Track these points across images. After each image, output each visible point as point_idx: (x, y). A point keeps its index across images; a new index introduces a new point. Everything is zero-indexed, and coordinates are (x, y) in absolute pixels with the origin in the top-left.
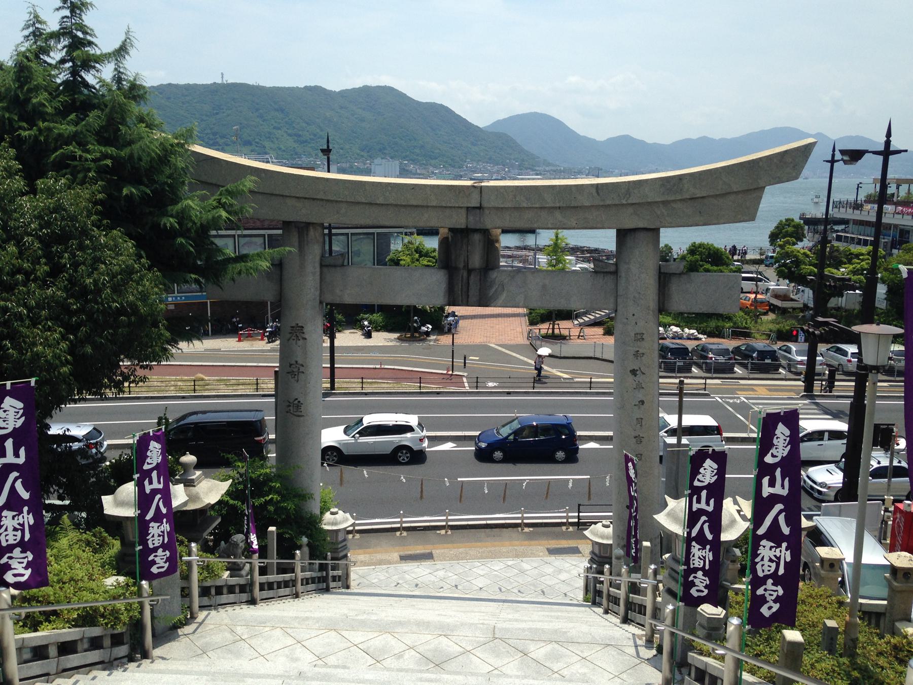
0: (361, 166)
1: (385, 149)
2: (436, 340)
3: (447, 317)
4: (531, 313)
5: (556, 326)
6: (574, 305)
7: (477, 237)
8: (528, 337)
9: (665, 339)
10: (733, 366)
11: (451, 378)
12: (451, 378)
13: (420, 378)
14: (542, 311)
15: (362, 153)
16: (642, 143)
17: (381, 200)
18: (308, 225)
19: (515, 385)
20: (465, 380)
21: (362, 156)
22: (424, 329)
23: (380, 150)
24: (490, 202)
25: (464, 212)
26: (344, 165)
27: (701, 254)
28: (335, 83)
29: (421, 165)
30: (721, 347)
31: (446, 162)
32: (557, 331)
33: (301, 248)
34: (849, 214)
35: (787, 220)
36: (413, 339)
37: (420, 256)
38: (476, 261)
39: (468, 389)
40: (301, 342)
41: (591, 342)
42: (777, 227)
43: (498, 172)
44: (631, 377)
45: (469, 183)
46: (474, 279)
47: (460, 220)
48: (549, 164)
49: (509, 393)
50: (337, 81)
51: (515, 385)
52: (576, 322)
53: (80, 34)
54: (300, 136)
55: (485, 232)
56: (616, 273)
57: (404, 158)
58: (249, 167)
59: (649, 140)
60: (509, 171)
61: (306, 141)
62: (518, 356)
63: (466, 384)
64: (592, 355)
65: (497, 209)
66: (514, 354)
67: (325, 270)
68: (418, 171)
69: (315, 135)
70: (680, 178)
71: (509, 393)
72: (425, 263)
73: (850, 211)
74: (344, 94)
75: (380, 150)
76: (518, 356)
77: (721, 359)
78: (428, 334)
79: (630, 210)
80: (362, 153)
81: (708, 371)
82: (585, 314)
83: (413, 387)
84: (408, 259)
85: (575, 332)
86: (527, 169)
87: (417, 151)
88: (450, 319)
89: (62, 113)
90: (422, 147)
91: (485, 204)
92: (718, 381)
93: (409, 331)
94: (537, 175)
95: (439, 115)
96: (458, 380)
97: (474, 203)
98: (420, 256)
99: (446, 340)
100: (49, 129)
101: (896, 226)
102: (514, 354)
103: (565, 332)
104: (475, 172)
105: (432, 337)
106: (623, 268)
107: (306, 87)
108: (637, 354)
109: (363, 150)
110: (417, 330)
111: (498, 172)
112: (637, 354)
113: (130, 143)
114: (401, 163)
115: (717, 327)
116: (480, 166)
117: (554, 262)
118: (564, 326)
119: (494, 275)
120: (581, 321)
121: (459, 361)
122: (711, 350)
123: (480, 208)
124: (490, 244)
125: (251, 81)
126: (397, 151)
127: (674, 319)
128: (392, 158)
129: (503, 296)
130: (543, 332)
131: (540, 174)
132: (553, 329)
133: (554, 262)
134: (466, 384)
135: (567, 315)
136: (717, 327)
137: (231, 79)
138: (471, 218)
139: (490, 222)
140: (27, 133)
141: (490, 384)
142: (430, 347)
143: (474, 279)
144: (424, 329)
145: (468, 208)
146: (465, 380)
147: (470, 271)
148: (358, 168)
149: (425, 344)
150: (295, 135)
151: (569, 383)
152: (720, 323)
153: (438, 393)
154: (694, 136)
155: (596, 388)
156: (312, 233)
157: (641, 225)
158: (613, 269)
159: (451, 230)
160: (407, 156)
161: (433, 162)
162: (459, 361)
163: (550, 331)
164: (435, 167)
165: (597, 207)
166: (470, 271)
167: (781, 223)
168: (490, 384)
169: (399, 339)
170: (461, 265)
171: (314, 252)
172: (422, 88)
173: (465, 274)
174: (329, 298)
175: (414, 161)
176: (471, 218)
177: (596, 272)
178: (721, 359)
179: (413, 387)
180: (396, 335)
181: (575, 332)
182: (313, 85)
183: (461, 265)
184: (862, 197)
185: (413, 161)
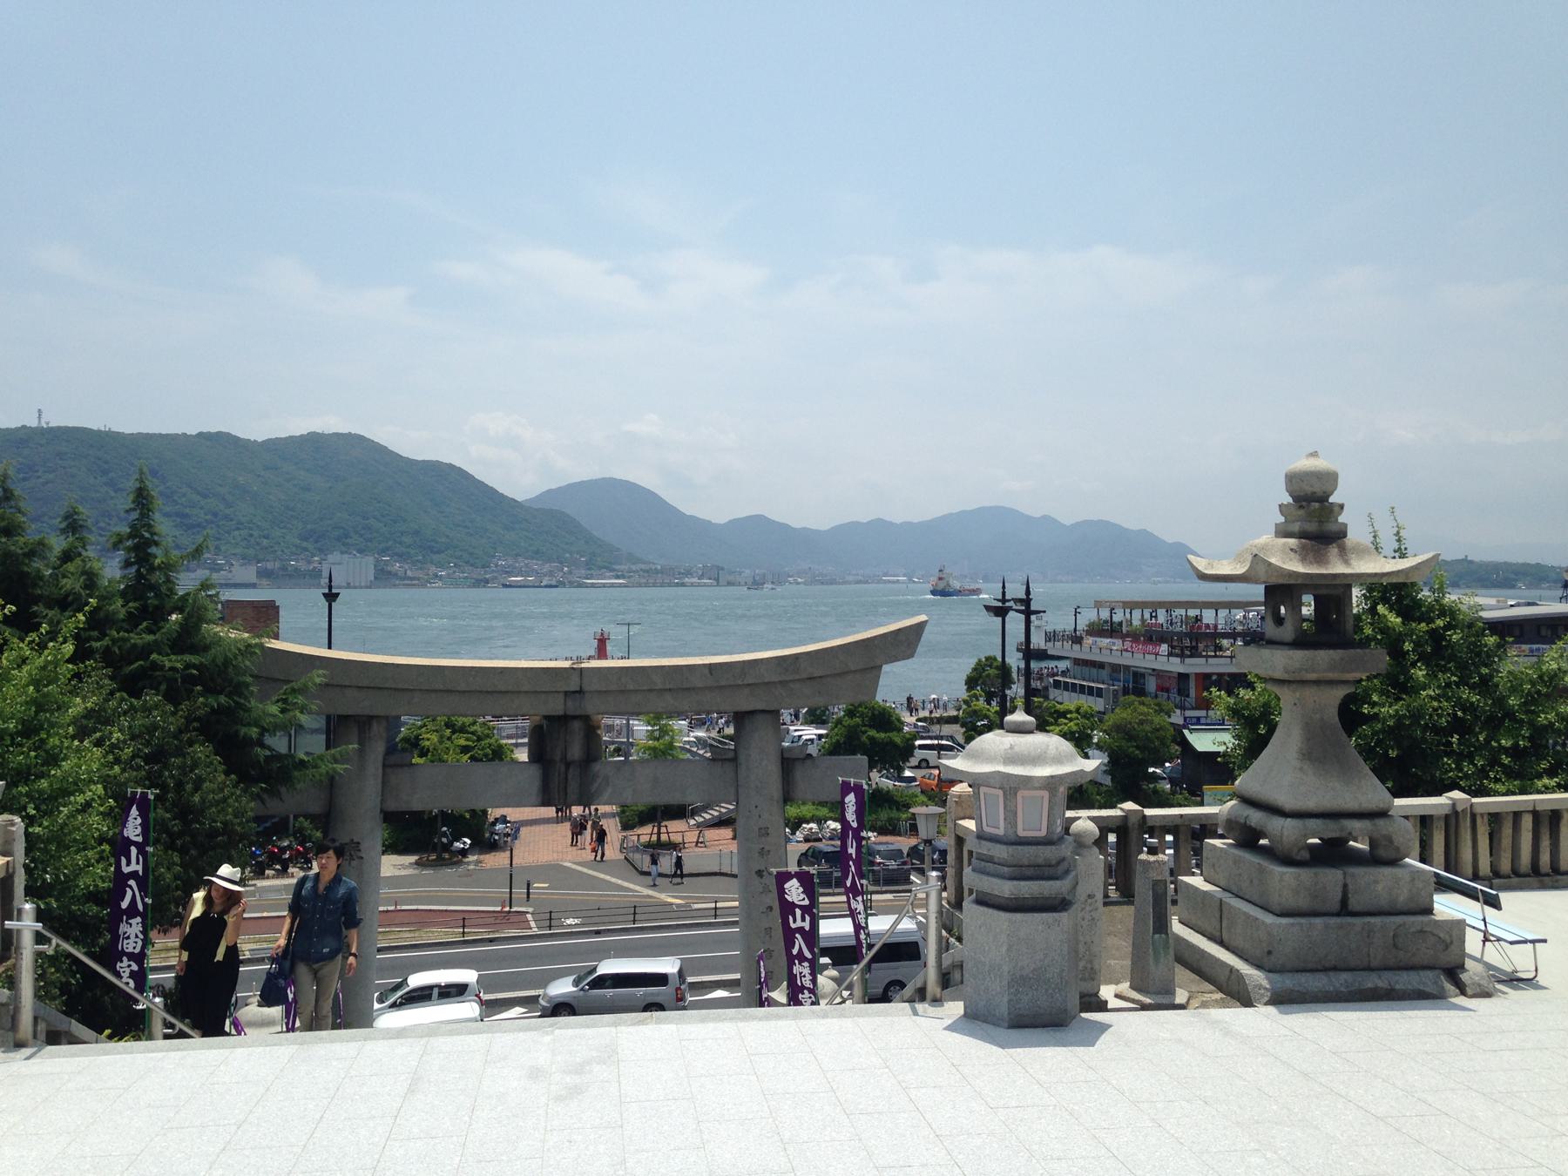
0: (303, 566)
1: (347, 536)
2: (478, 862)
3: (494, 824)
4: (623, 812)
5: (663, 830)
6: (692, 798)
7: (576, 725)
8: (622, 848)
9: (819, 840)
10: (908, 873)
11: (506, 918)
12: (506, 918)
13: (464, 920)
14: (641, 808)
15: (305, 544)
16: (785, 527)
17: (463, 687)
18: (371, 718)
19: (606, 919)
20: (529, 917)
21: (306, 549)
22: (458, 845)
23: (338, 539)
24: (591, 685)
25: (562, 696)
26: (270, 565)
27: (862, 716)
28: (256, 428)
29: (414, 563)
30: (891, 847)
31: (459, 558)
32: (664, 837)
33: (361, 743)
34: (1066, 649)
35: (987, 659)
36: (440, 863)
37: (453, 732)
38: (576, 751)
39: (535, 931)
40: (354, 863)
41: (715, 850)
42: (974, 670)
43: (551, 574)
44: (757, 880)
45: (567, 664)
46: (573, 772)
47: (556, 707)
48: (639, 561)
49: (598, 933)
50: (259, 424)
51: (606, 919)
52: (692, 822)
53: (147, 535)
54: (186, 516)
55: (586, 719)
56: (734, 760)
57: (383, 552)
58: (301, 655)
59: (796, 523)
60: (570, 572)
61: (199, 525)
62: (608, 878)
63: (533, 924)
64: (716, 869)
65: (600, 692)
66: (602, 876)
67: (389, 770)
68: (409, 573)
69: (215, 515)
70: (796, 657)
71: (598, 933)
72: (462, 742)
73: (1068, 645)
74: (273, 446)
75: (338, 539)
76: (608, 878)
77: (892, 864)
78: (464, 853)
79: (746, 691)
80: (305, 544)
81: (876, 882)
82: (705, 808)
83: (453, 934)
84: (435, 738)
85: (692, 837)
86: (600, 568)
87: (407, 540)
88: (499, 827)
89: (133, 621)
90: (417, 533)
91: (586, 688)
92: (889, 896)
93: (434, 849)
94: (618, 577)
95: (446, 483)
96: (521, 918)
97: (574, 687)
98: (453, 732)
99: (496, 861)
100: (124, 640)
101: (1127, 668)
102: (602, 876)
103: (676, 838)
104: (510, 574)
105: (471, 858)
106: (742, 758)
107: (200, 434)
108: (762, 852)
109: (306, 539)
110: (447, 848)
111: (551, 574)
112: (762, 852)
113: (206, 648)
114: (377, 561)
115: (890, 820)
116: (521, 563)
117: (657, 734)
118: (675, 829)
119: (596, 767)
120: (700, 819)
121: (520, 891)
122: (879, 852)
123: (581, 692)
124: (591, 731)
125: (94, 425)
126: (370, 540)
127: (831, 810)
128: (360, 551)
129: (606, 795)
130: (645, 839)
131: (623, 577)
132: (659, 833)
133: (657, 734)
134: (533, 924)
135: (679, 812)
136: (890, 820)
137: (57, 418)
138: (570, 703)
139: (590, 706)
140: (99, 644)
141: (569, 921)
142: (469, 874)
143: (573, 772)
144: (458, 845)
145: (566, 693)
146: (529, 917)
147: (568, 765)
148: (296, 570)
149: (461, 869)
150: (178, 514)
151: (685, 911)
152: (894, 814)
153: (491, 941)
154: (864, 518)
155: (723, 916)
156: (375, 726)
157: (759, 707)
158: (731, 755)
159: (546, 717)
160: (388, 549)
161: (435, 557)
162: (520, 891)
163: (654, 838)
164: (441, 566)
165: (710, 689)
166: (568, 765)
167: (979, 663)
168: (569, 921)
169: (417, 863)
170: (558, 758)
171: (378, 749)
172: (412, 438)
173: (563, 769)
174: (392, 806)
175: (401, 557)
176: (570, 703)
177: (713, 760)
178: (892, 864)
179: (453, 934)
180: (413, 859)
181: (692, 837)
182: (214, 430)
183: (558, 758)
184: (1082, 624)
185: (400, 555)
